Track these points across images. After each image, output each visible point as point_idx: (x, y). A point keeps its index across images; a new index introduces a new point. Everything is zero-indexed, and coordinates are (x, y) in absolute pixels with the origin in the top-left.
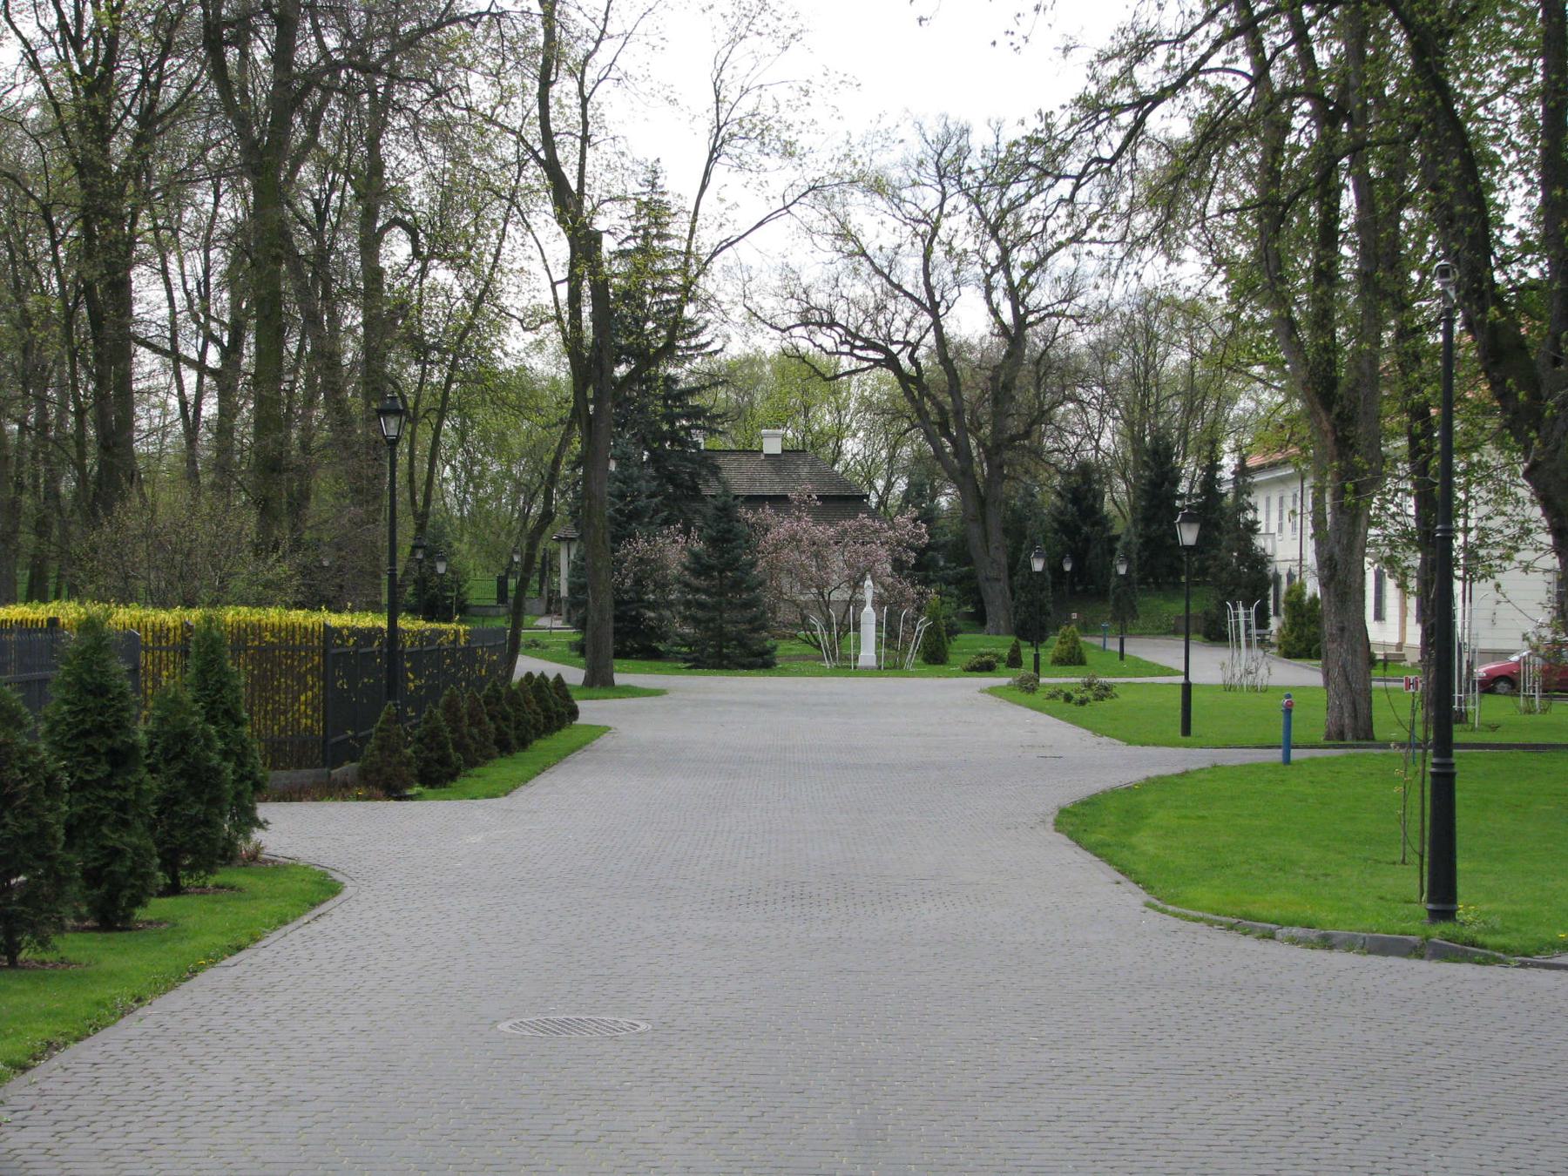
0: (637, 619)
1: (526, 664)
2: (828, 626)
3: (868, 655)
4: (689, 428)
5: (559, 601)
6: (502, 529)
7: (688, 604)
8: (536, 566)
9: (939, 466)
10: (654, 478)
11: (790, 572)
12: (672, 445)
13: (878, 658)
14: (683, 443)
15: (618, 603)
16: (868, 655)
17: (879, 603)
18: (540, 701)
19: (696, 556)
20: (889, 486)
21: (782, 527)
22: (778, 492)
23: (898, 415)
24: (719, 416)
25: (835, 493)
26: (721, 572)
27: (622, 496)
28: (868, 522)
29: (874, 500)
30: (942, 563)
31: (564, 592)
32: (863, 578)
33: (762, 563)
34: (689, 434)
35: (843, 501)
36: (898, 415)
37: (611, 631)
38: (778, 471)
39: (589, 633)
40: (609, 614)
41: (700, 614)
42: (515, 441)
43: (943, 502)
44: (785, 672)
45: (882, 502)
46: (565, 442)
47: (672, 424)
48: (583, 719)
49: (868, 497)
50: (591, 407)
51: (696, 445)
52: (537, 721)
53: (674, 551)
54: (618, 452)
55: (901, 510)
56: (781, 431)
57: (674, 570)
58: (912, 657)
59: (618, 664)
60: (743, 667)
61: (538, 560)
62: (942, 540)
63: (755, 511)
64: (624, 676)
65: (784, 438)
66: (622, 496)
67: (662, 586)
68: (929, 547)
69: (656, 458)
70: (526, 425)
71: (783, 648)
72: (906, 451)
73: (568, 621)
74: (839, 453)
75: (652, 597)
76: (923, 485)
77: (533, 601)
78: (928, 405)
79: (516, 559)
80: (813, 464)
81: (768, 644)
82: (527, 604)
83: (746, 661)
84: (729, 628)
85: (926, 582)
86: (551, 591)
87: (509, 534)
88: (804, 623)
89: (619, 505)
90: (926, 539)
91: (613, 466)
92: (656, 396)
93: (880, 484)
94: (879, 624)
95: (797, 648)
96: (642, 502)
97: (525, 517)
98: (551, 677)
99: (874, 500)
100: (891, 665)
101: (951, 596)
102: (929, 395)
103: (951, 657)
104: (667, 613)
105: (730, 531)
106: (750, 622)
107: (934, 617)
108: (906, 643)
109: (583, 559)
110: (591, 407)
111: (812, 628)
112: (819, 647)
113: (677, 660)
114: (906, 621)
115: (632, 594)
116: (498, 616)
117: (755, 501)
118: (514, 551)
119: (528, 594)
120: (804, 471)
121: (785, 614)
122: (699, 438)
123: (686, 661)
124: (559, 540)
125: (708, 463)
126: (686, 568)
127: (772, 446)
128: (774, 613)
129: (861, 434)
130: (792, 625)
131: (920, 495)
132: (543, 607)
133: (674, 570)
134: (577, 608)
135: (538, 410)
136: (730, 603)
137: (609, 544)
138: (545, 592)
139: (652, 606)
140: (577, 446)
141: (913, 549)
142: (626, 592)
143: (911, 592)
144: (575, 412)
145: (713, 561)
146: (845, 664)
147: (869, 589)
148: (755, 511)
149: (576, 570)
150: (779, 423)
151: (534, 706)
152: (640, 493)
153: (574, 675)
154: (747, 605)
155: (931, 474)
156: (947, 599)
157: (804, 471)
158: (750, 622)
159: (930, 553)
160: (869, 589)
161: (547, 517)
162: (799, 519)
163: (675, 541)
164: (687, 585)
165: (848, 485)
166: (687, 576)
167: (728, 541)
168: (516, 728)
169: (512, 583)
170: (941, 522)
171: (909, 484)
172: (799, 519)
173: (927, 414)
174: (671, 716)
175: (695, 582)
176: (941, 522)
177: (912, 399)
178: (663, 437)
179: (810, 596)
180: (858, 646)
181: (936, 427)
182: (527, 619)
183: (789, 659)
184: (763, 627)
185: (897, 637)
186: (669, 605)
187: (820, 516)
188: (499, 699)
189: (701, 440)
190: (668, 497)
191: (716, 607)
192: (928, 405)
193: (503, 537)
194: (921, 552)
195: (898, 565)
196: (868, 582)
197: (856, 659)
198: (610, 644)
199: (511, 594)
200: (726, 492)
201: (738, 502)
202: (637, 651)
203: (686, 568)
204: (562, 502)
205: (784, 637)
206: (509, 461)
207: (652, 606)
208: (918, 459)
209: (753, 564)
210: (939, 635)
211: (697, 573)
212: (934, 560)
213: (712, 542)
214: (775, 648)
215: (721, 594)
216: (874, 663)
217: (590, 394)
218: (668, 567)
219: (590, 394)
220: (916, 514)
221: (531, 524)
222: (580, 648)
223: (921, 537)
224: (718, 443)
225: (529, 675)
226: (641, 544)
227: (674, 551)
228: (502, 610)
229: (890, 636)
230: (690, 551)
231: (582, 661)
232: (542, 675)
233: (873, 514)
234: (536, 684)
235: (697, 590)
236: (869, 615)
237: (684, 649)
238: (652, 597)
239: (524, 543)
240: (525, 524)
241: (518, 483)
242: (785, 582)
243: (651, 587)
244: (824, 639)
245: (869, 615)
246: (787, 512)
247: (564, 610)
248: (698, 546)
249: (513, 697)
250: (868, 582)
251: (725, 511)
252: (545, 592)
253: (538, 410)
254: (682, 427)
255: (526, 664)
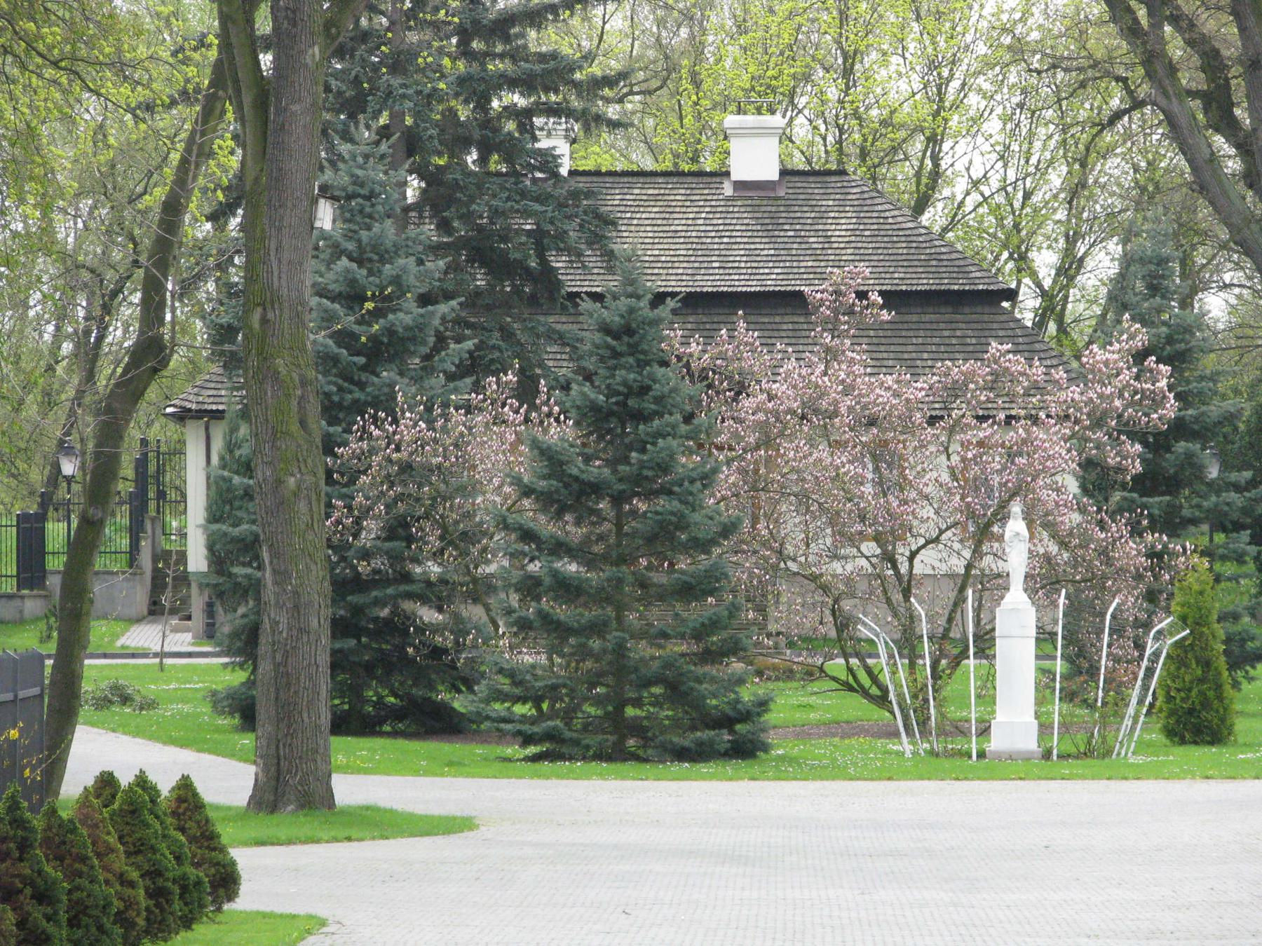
0: (398, 627)
1: (98, 752)
2: (908, 644)
3: (1016, 718)
4: (528, 113)
5: (183, 579)
6: (27, 387)
7: (530, 588)
8: (120, 489)
9: (1204, 212)
10: (436, 250)
11: (803, 499)
12: (483, 160)
13: (1044, 729)
14: (511, 149)
15: (345, 586)
16: (1016, 718)
17: (1044, 581)
18: (137, 849)
19: (550, 458)
20: (1070, 268)
21: (782, 374)
22: (771, 285)
23: (1094, 71)
24: (608, 81)
25: (925, 283)
26: (618, 500)
27: (353, 297)
28: (1016, 364)
29: (1028, 307)
30: (1213, 472)
31: (197, 560)
32: (1002, 515)
33: (728, 477)
34: (527, 129)
35: (948, 306)
36: (1094, 71)
37: (324, 659)
38: (770, 227)
39: (265, 667)
40: (319, 619)
41: (562, 612)
42: (63, 157)
43: (1216, 306)
44: (794, 769)
45: (1052, 306)
46: (198, 151)
47: (482, 103)
48: (247, 899)
49: (1011, 295)
50: (266, 60)
51: (548, 161)
52: (130, 904)
53: (493, 449)
54: (342, 179)
55: (1104, 331)
56: (778, 120)
57: (492, 497)
58: (1135, 724)
59: (342, 748)
60: (682, 755)
61: (127, 470)
62: (1215, 409)
63: (709, 338)
64: (364, 777)
65: (786, 137)
66: (353, 297)
67: (461, 539)
68: (1179, 428)
69: (442, 196)
70: (90, 110)
71: (788, 705)
72: (1115, 169)
73: (210, 633)
74: (936, 174)
75: (434, 569)
76: (1162, 261)
77: (116, 583)
78: (1176, 48)
79: (68, 468)
80: (863, 205)
81: (747, 694)
82: (98, 588)
83: (688, 740)
84: (641, 650)
85: (1172, 524)
86: (160, 556)
87: (49, 401)
88: (843, 635)
89: (348, 321)
90: (1171, 408)
91: (325, 216)
92: (436, 26)
93: (1045, 261)
94: (1044, 637)
95: (826, 703)
96: (407, 315)
97: (89, 354)
98: (165, 785)
99: (1028, 307)
100: (1077, 747)
101: (1240, 559)
102: (1175, 20)
103: (1240, 725)
104: (475, 613)
105: (644, 390)
106: (699, 634)
107: (1194, 619)
108: (1116, 686)
109: (247, 468)
110: (266, 60)
111: (863, 650)
112: (882, 700)
113: (501, 737)
114: (1117, 631)
115: (378, 563)
116: (20, 621)
117: (706, 306)
118: (64, 448)
119: (99, 563)
120: (841, 227)
121: (793, 611)
122: (554, 140)
123: (527, 740)
124: (183, 416)
125: (582, 209)
126: (527, 492)
127: (755, 158)
128: (761, 609)
129: (993, 126)
130: (810, 642)
131: (1155, 288)
132: (140, 596)
133: (492, 497)
134: (233, 601)
135: (121, 67)
136: (643, 584)
137: (319, 426)
138: (145, 559)
139: (434, 593)
140: (228, 158)
141: (1133, 436)
142: (366, 555)
143: (1131, 552)
144: (223, 74)
145: (597, 470)
146: (951, 742)
147: (1017, 547)
148: (709, 338)
149: (224, 503)
150: (766, 96)
151: (119, 861)
152: (401, 289)
153: (227, 780)
154: (689, 591)
155: (1186, 231)
156: (1229, 569)
157: (841, 227)
158: (698, 635)
159: (1181, 446)
160: (1017, 547)
161: (150, 354)
162: (831, 355)
163: (500, 421)
164: (527, 535)
165: (960, 265)
166: (530, 513)
167: (641, 417)
168: (73, 923)
169: (57, 532)
170: (1209, 363)
171: (1127, 261)
172: (831, 355)
173: (1172, 69)
174: (1034, 609)
175: (545, 526)
176: (1209, 363)
177: (1132, 31)
178: (458, 141)
179: (860, 560)
180: (987, 696)
181: (1196, 104)
182: (98, 632)
183: (803, 732)
184: (734, 649)
185: (1093, 672)
186: (479, 590)
187: (887, 349)
188: (24, 846)
189: (563, 148)
190: (474, 300)
191: (602, 597)
192: (1176, 48)
193: (31, 409)
194: (1157, 443)
195: (1097, 480)
196: (1016, 526)
197: (984, 731)
198: (322, 704)
199: (55, 563)
200: (631, 287)
201: (664, 311)
202: (398, 714)
203: (527, 492)
204: (190, 324)
205: (789, 675)
206: (46, 207)
207: (434, 593)
208: (1147, 192)
209: (707, 479)
210: (1207, 664)
211: (551, 503)
212: (1192, 465)
213: (596, 419)
214: (763, 705)
215: (622, 560)
216: (1029, 742)
217: (264, 23)
218: (472, 488)
219: (264, 23)
220: (1142, 338)
221: (107, 374)
222: (244, 710)
223: (1157, 401)
224: (604, 153)
225: (106, 782)
226: (410, 427)
227: (493, 449)
228: (32, 606)
229: (1076, 668)
230: (535, 444)
231: (247, 741)
232: (142, 781)
233: (1028, 342)
234: (123, 803)
235: (559, 548)
236: (1017, 618)
237: (520, 709)
238: (434, 569)
239: (89, 425)
240: (90, 376)
241: (70, 265)
242: (792, 524)
243: (434, 541)
244: (894, 674)
245: (1017, 618)
246: (795, 338)
247: (197, 603)
248: (561, 433)
249: (61, 841)
250: (1016, 526)
251: (628, 339)
252: (145, 559)
253: (121, 67)
254: (510, 111)
255: (98, 752)
